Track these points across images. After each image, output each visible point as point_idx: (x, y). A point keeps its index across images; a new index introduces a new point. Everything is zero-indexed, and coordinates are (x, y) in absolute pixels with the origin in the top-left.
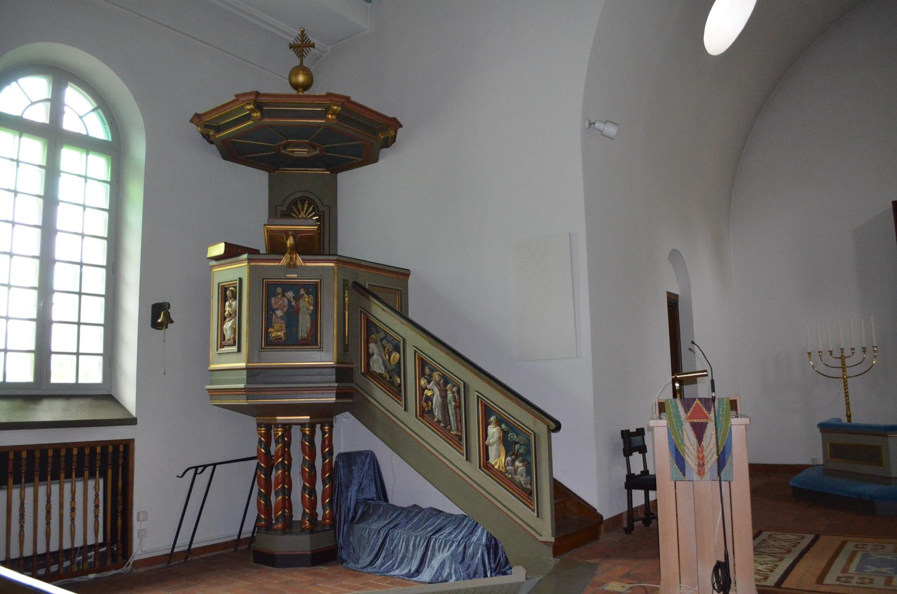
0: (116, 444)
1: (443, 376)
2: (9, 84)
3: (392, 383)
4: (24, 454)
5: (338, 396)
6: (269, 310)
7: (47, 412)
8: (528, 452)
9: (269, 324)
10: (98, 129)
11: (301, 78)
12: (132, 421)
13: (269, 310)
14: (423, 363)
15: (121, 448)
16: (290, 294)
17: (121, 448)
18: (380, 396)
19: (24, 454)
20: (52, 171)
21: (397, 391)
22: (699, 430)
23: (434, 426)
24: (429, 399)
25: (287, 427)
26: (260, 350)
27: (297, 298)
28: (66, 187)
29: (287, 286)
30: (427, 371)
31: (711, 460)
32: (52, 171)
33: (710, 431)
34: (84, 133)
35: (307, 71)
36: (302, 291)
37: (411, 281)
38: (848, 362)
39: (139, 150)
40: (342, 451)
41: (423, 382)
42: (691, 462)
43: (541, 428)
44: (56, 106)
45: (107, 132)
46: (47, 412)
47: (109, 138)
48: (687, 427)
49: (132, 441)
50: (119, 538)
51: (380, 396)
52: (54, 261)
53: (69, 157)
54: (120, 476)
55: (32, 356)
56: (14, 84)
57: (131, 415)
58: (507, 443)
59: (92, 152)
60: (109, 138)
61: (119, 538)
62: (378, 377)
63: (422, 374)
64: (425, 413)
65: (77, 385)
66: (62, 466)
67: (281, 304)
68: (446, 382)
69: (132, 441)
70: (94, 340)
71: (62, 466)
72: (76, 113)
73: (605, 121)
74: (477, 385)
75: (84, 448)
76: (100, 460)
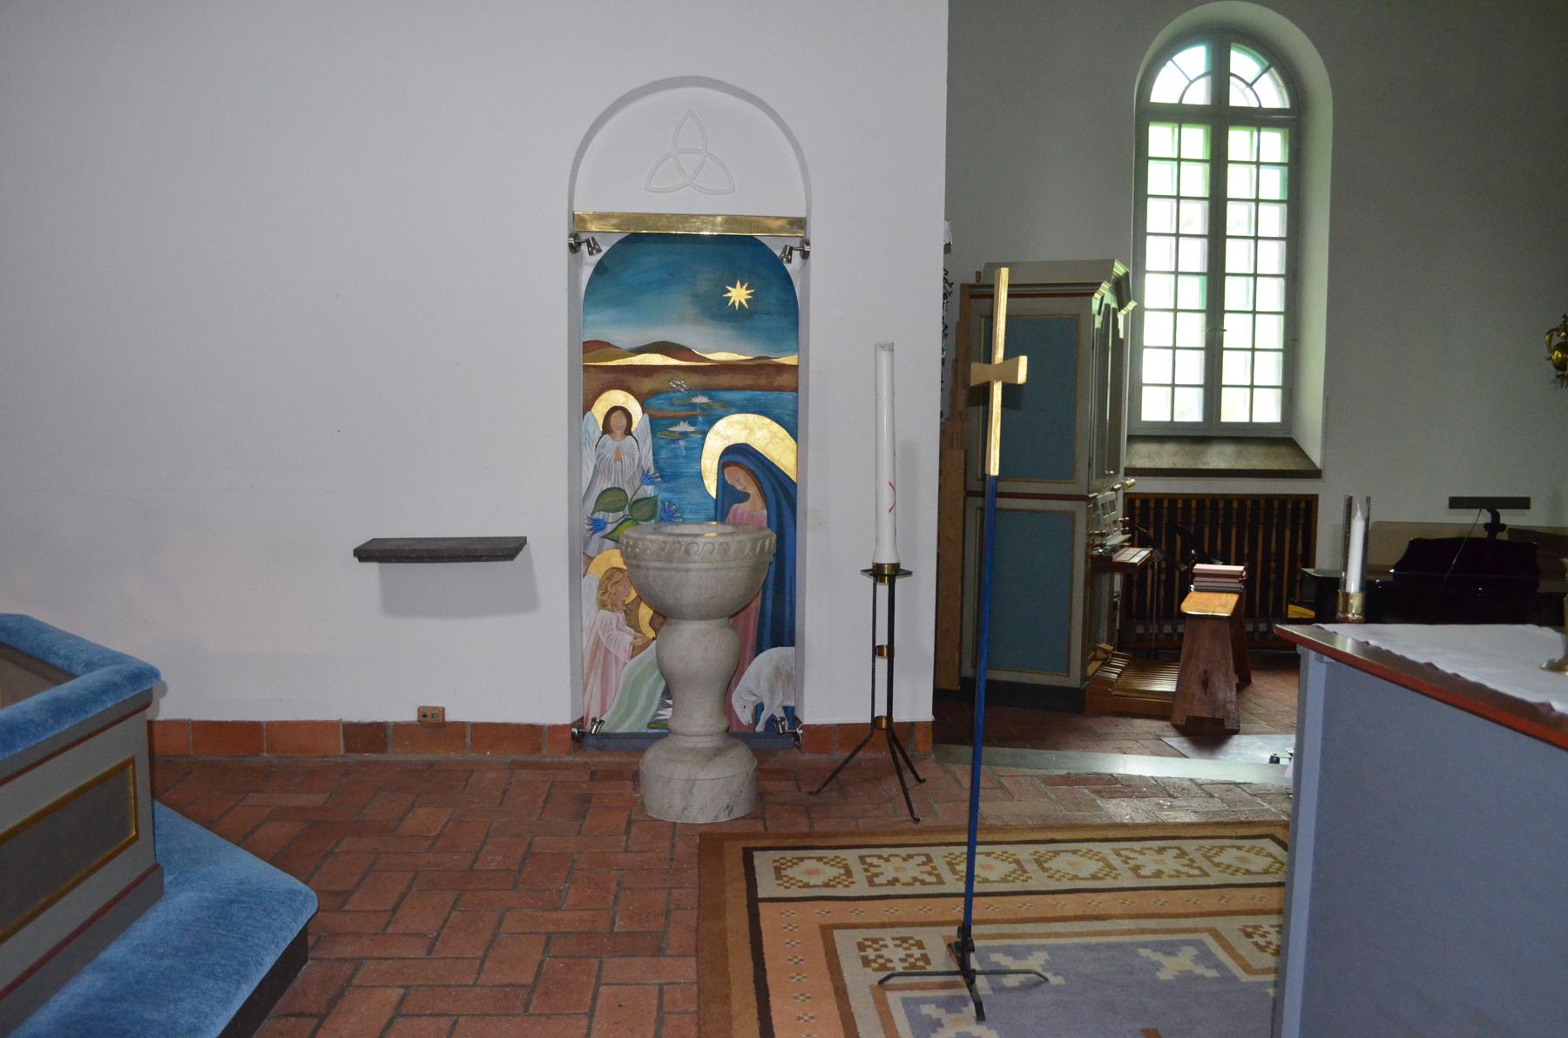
0: (1296, 499)
2: (1164, 64)
4: (1249, 503)
7: (1218, 457)
10: (1271, 94)
12: (1315, 474)
15: (1303, 505)
17: (1303, 505)
19: (1249, 503)
20: (1218, 161)
28: (1238, 182)
32: (1218, 161)
34: (1256, 105)
40: (1378, 519)
44: (1220, 75)
45: (1283, 98)
46: (1218, 457)
47: (1285, 104)
50: (1271, 608)
52: (1144, 272)
53: (1239, 141)
54: (1219, 537)
55: (1201, 391)
56: (1169, 63)
59: (1186, 125)
60: (1285, 104)
61: (1271, 608)
65: (1250, 425)
66: (1234, 520)
70: (1270, 369)
71: (1234, 520)
72: (1187, 77)
75: (1299, 502)
76: (1140, 516)
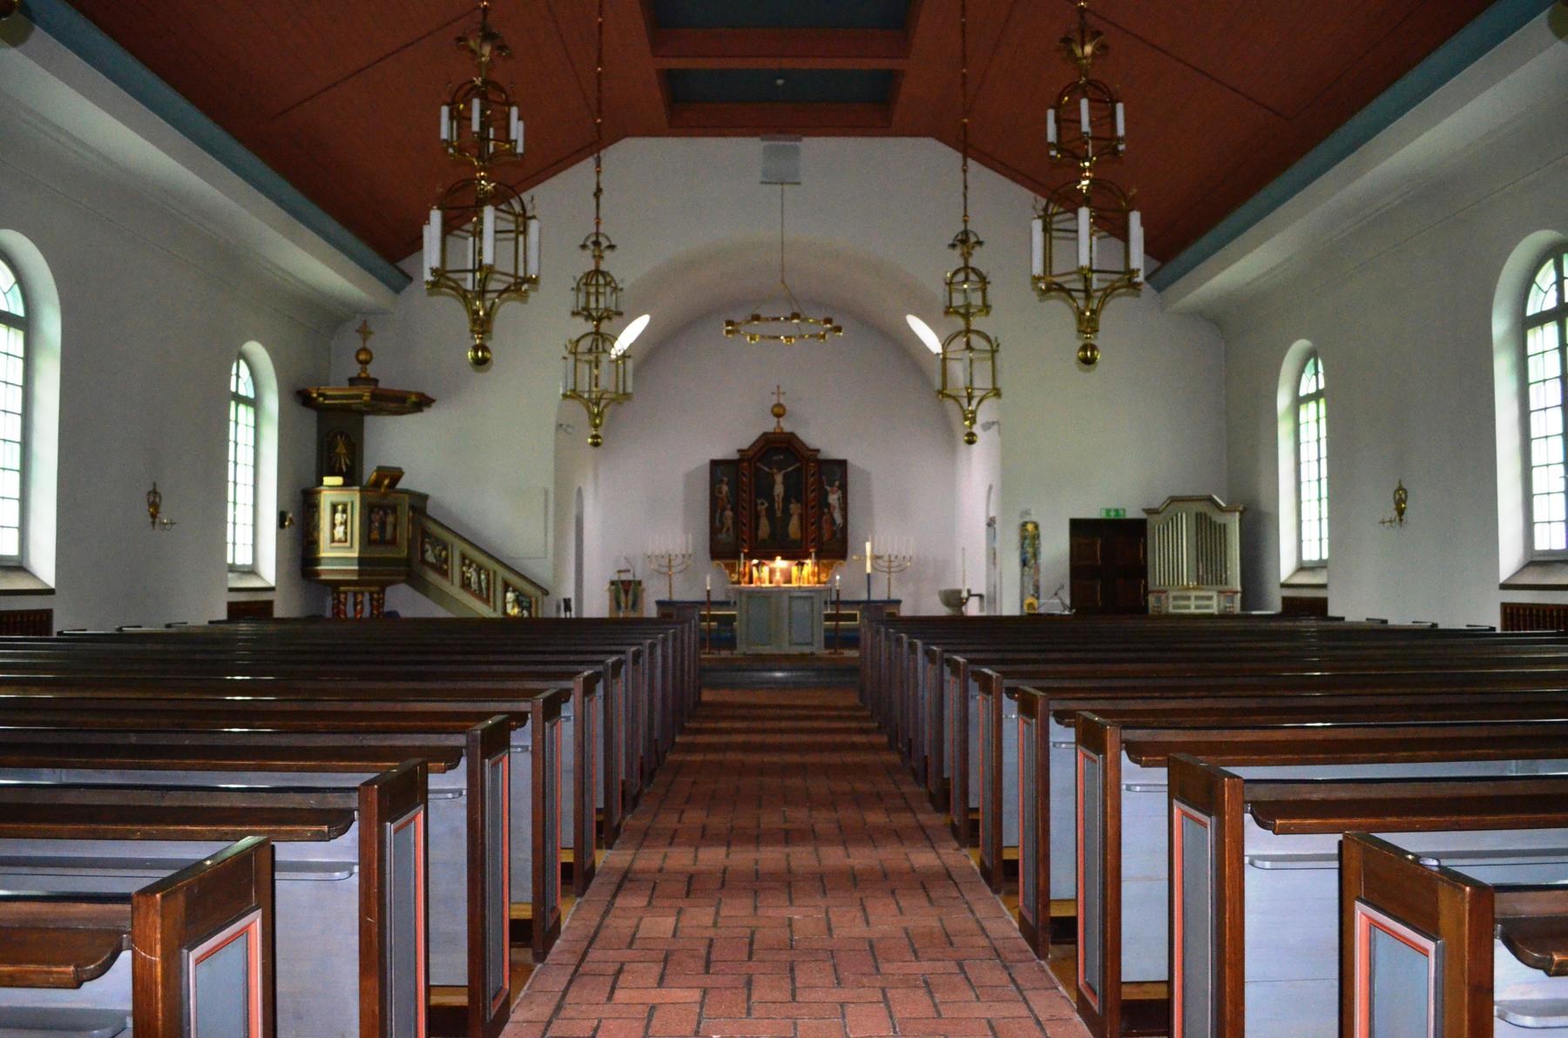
1: (477, 566)
3: (441, 568)
5: (359, 575)
6: (371, 522)
8: (531, 606)
9: (370, 531)
11: (362, 357)
13: (371, 522)
14: (463, 557)
16: (381, 513)
18: (433, 577)
21: (444, 574)
22: (626, 592)
23: (473, 593)
24: (469, 579)
25: (345, 593)
26: (348, 544)
27: (386, 514)
29: (381, 507)
30: (467, 562)
31: (630, 603)
33: (631, 592)
34: (7, 310)
35: (368, 352)
36: (389, 511)
37: (429, 503)
38: (673, 563)
39: (51, 325)
41: (465, 569)
42: (623, 605)
43: (539, 593)
48: (622, 591)
49: (51, 611)
51: (433, 577)
57: (47, 585)
58: (518, 602)
62: (432, 566)
63: (463, 564)
64: (465, 585)
67: (376, 517)
68: (480, 569)
69: (51, 611)
73: (626, 967)
74: (503, 573)
